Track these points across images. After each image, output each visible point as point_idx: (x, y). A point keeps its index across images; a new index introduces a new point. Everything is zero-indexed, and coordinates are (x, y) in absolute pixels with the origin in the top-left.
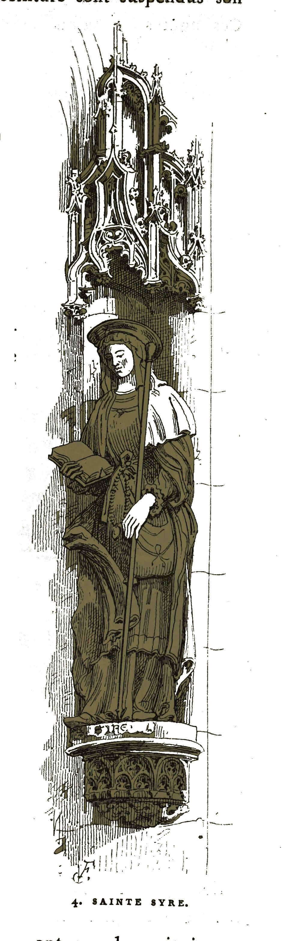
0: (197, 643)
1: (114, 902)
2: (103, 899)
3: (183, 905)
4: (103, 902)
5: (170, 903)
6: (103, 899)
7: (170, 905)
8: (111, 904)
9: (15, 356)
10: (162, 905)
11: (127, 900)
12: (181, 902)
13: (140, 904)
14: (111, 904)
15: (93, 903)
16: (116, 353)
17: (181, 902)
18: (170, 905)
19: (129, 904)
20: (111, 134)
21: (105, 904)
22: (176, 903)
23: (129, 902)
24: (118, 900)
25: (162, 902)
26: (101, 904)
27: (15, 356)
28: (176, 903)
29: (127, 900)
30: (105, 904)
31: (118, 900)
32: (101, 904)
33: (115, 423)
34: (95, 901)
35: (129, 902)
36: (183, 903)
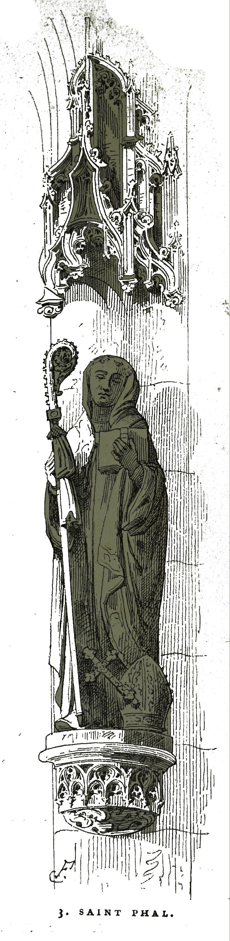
1: (102, 912)
2: (155, 911)
6: (155, 911)
8: (99, 914)
14: (99, 914)
23: (118, 913)
24: (106, 911)
25: (90, 913)
26: (153, 916)
31: (106, 911)
34: (81, 912)
35: (118, 913)
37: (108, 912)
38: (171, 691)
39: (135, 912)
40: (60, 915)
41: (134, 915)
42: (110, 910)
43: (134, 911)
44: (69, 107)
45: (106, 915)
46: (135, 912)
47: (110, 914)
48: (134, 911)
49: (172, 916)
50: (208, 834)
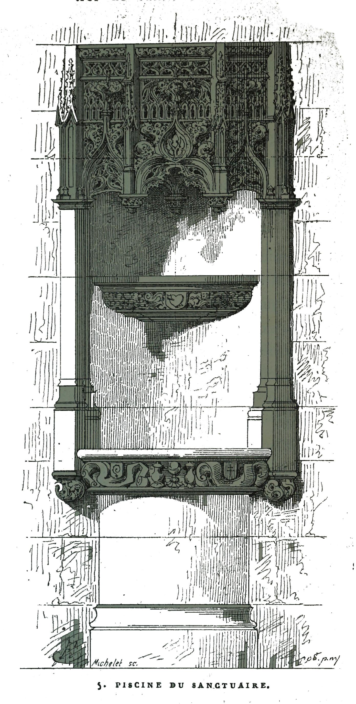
0: (159, 498)
1: (251, 686)
2: (201, 683)
3: (265, 687)
4: (201, 686)
5: (254, 686)
6: (201, 683)
7: (253, 687)
8: (248, 687)
9: (26, 461)
10: (225, 687)
11: (223, 684)
12: (158, 684)
13: (161, 687)
14: (248, 687)
15: (129, 687)
16: (43, 457)
17: (263, 684)
18: (253, 687)
19: (225, 687)
20: (176, 306)
21: (202, 687)
22: (259, 685)
23: (225, 686)
24: (149, 683)
25: (241, 686)
26: (199, 687)
27: (26, 461)
28: (259, 685)
29: (223, 684)
30: (202, 687)
31: (149, 683)
32: (199, 687)
33: (300, 307)
34: (194, 686)
35: (225, 686)
36: (265, 685)
37: (150, 685)
38: (169, 243)
39: (118, 684)
40: (99, 687)
41: (117, 687)
42: (152, 683)
43: (117, 683)
44: (330, 664)
45: (208, 687)
46: (118, 684)
47: (152, 687)
48: (117, 683)
49: (268, 687)
50: (37, 45)
